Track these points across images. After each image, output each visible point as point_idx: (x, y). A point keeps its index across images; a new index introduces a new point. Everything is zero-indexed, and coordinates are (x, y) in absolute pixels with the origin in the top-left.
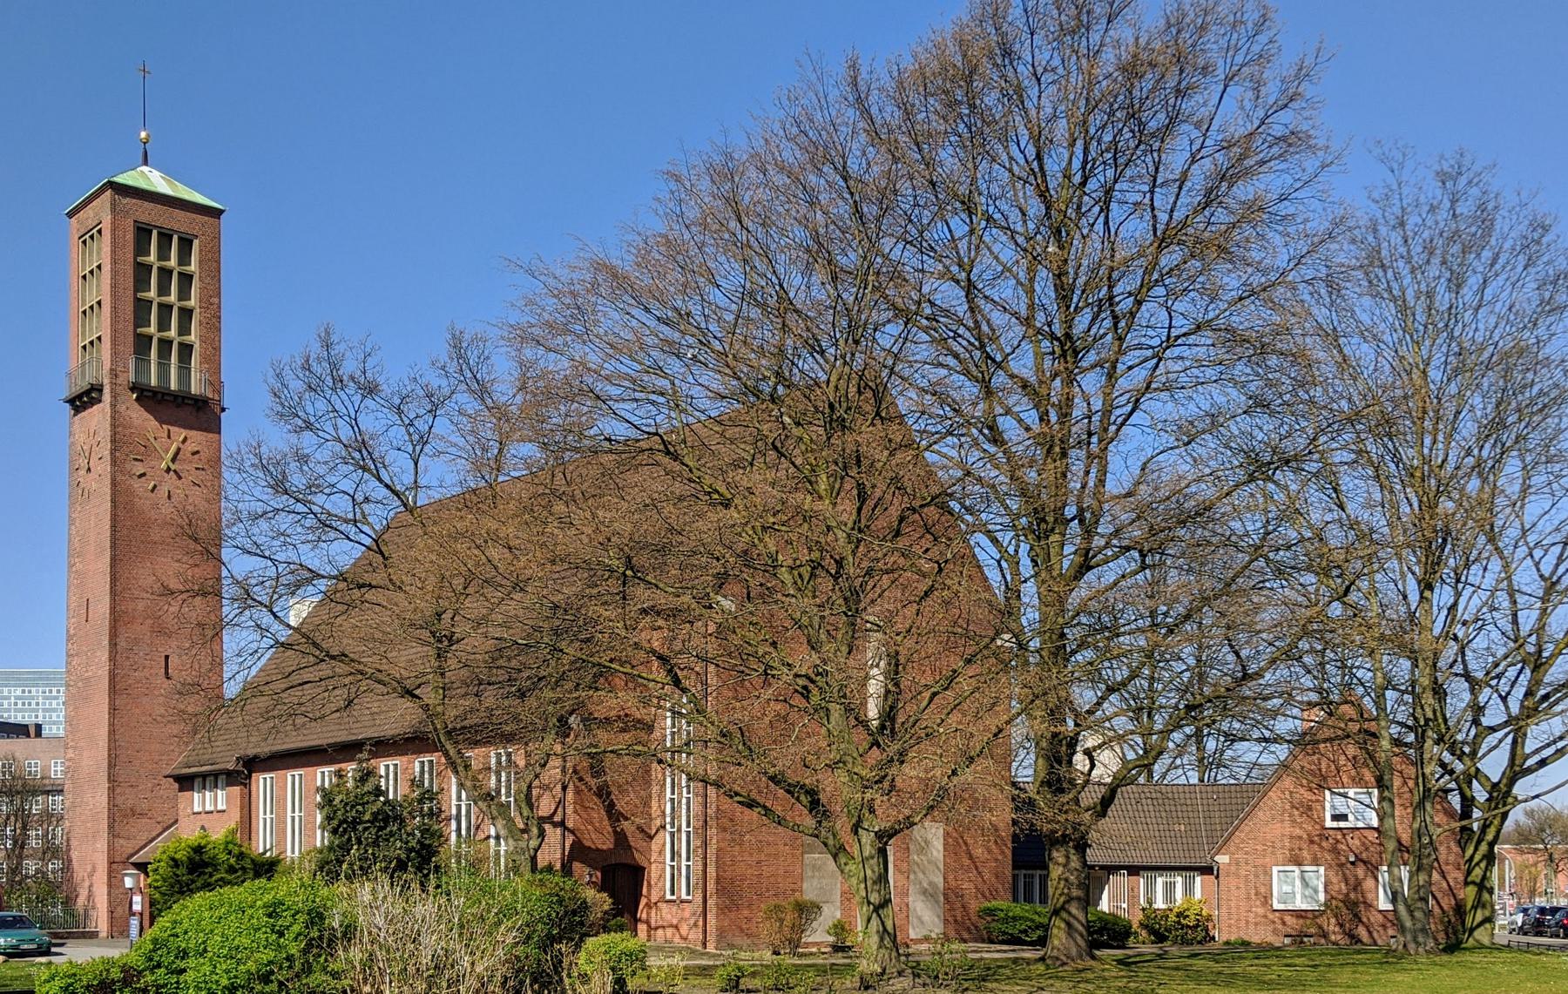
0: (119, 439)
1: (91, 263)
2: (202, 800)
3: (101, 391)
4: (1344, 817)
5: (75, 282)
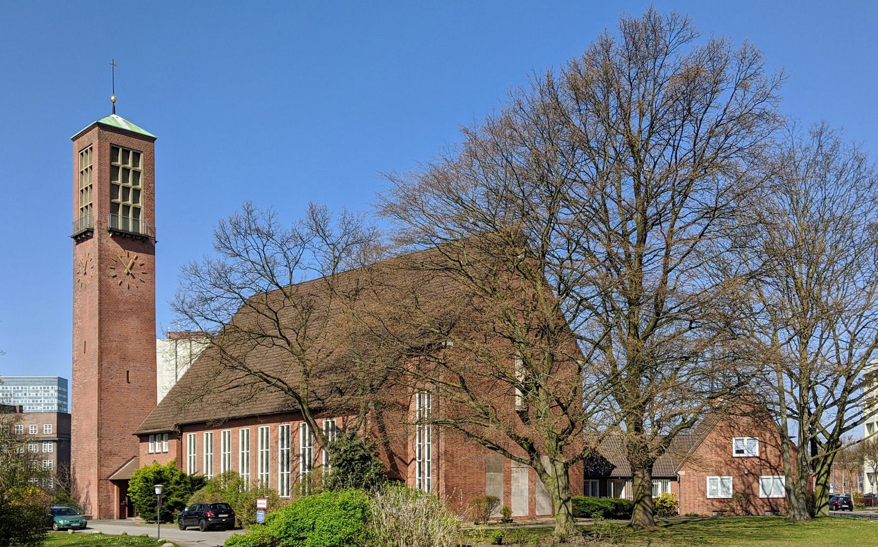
1: (86, 165)
2: (153, 447)
3: (92, 232)
4: (742, 452)
5: (76, 175)
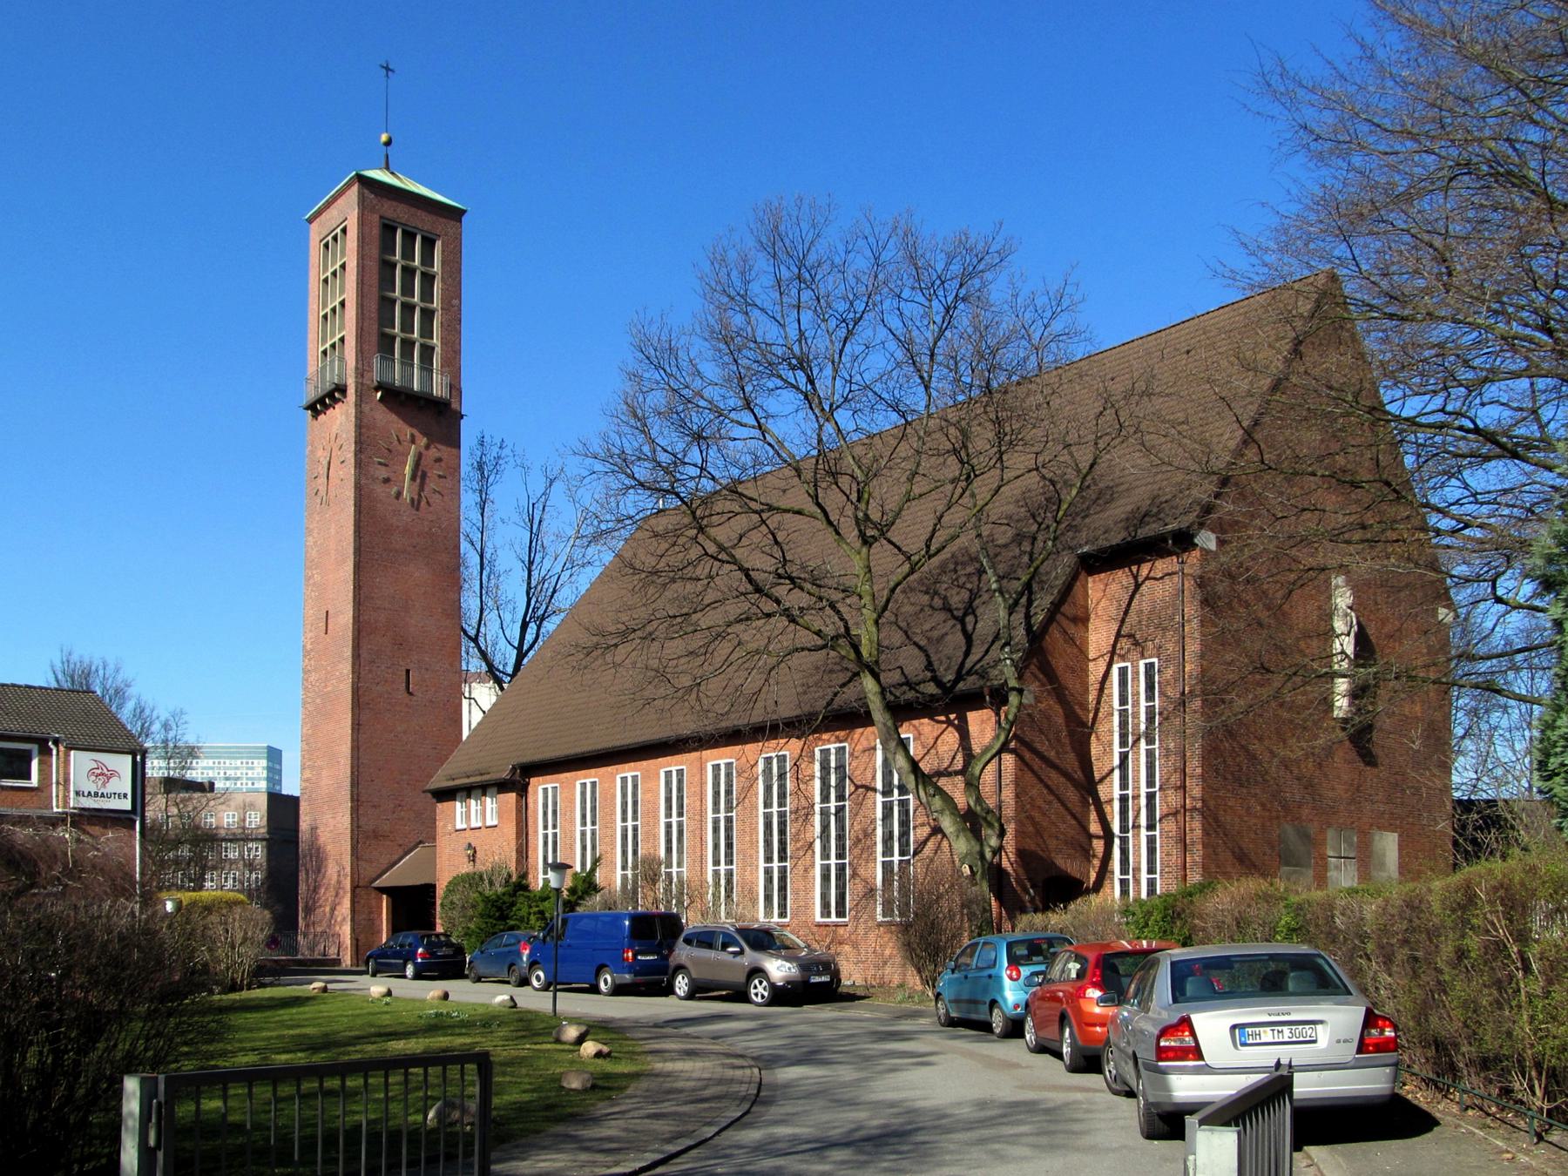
0: (361, 426)
1: (333, 335)
